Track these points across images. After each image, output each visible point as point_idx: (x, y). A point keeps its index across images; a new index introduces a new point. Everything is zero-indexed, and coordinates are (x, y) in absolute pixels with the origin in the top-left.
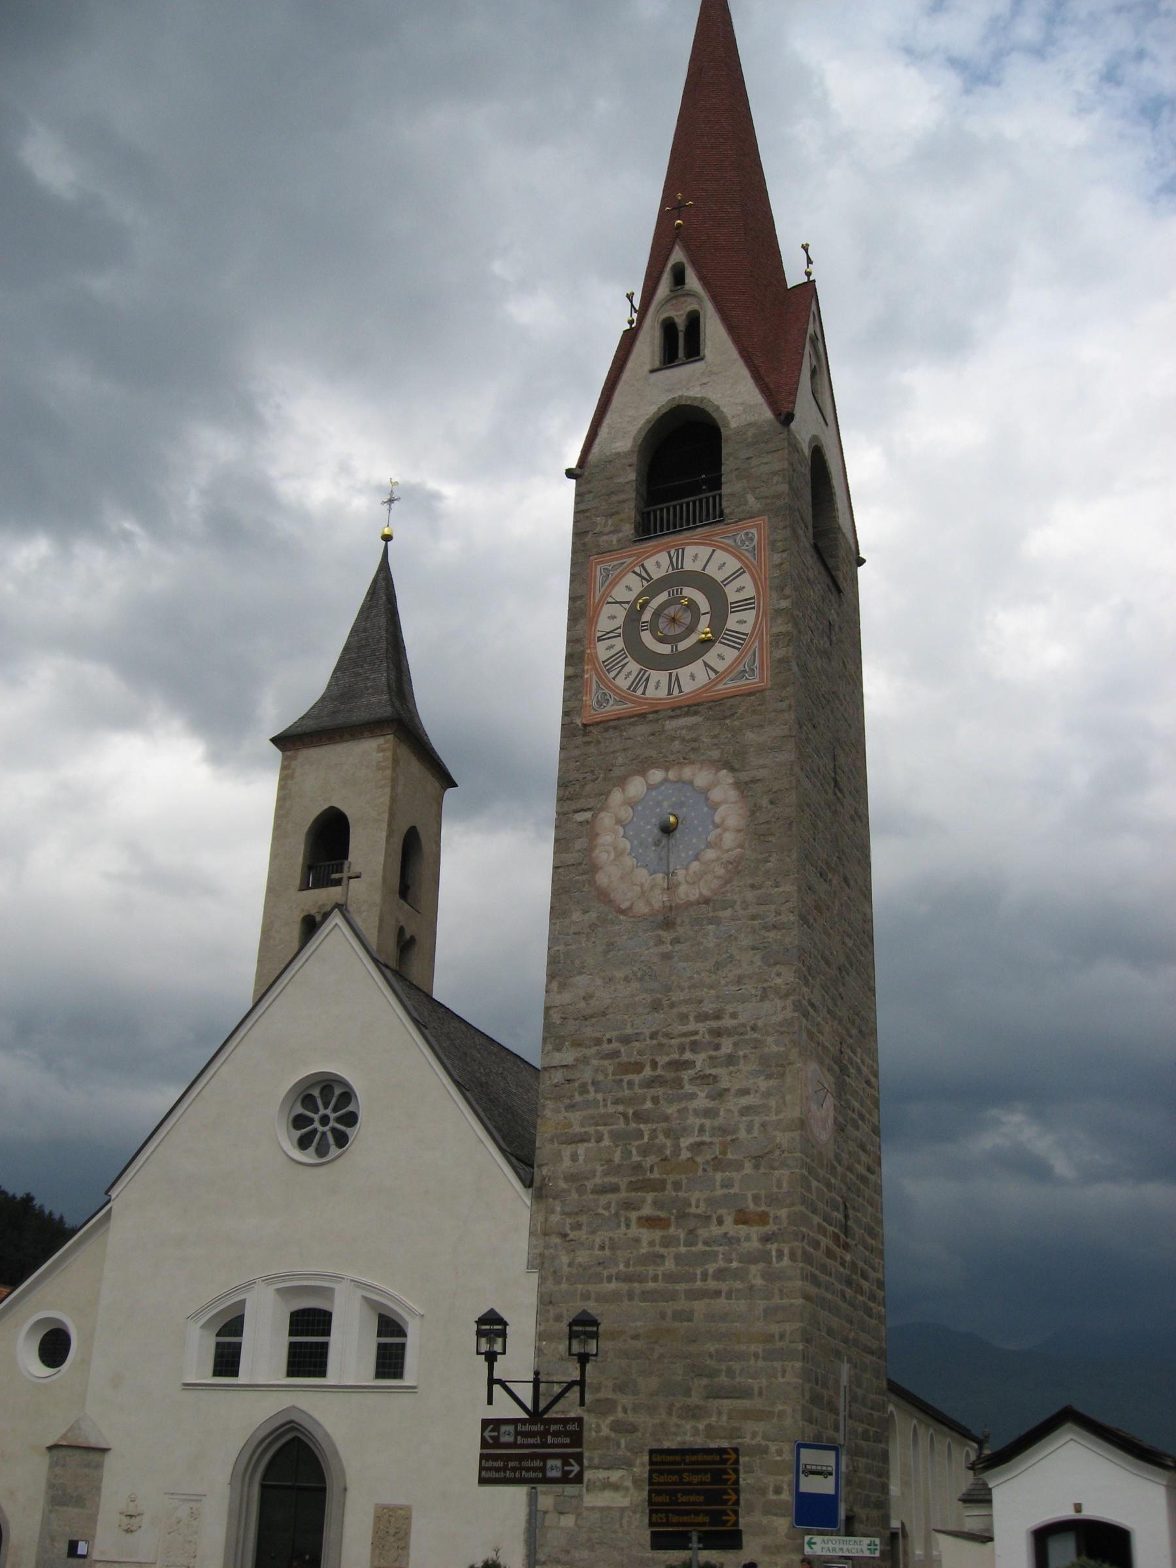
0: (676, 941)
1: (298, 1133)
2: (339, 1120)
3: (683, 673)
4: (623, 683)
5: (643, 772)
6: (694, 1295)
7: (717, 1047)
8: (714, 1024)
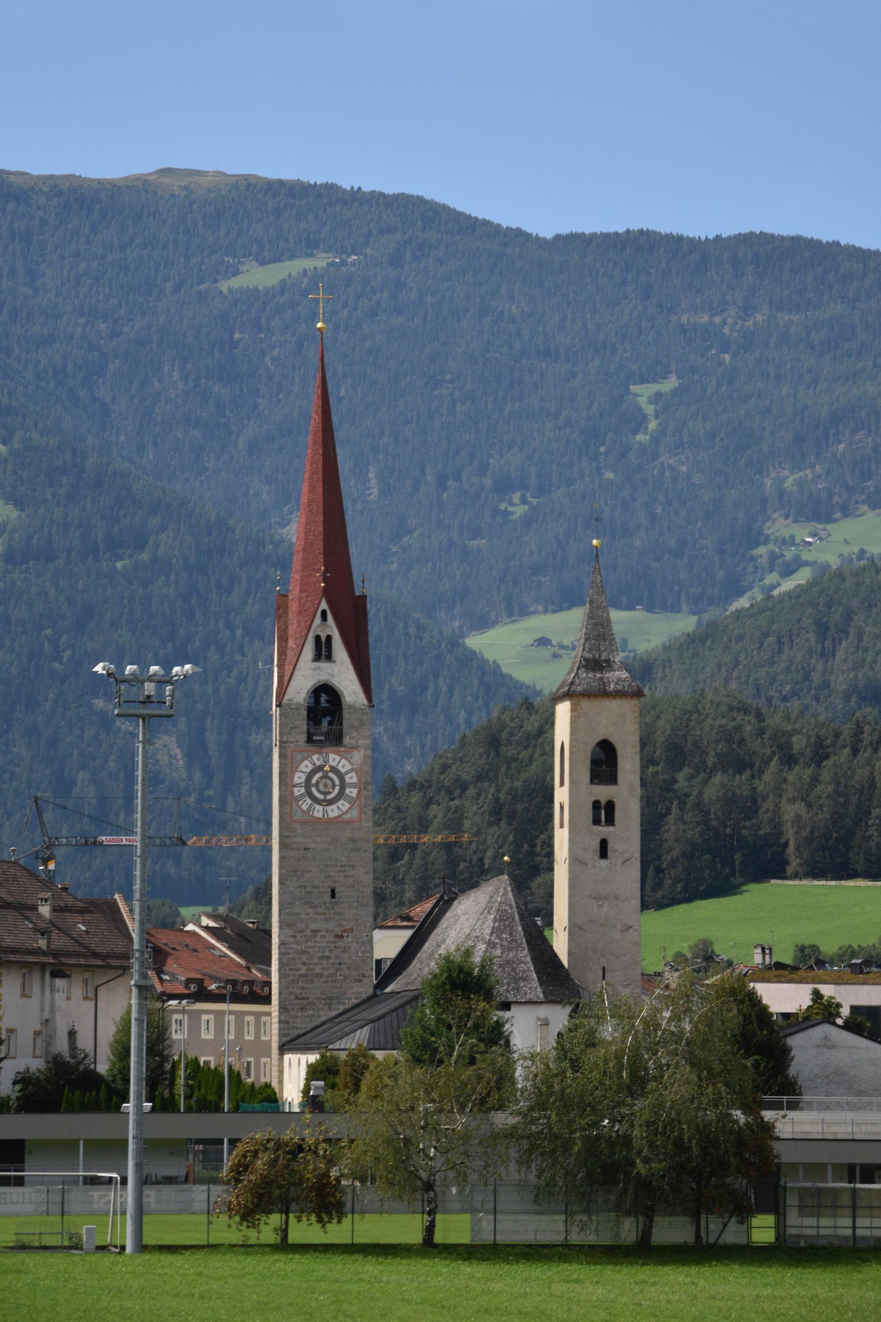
3: (329, 808)
4: (305, 807)
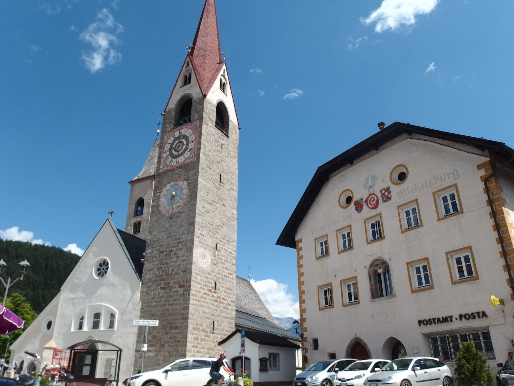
0: (173, 222)
1: (98, 272)
2: (100, 269)
3: (179, 159)
4: (168, 162)
5: (169, 183)
6: (169, 305)
7: (178, 246)
8: (178, 241)
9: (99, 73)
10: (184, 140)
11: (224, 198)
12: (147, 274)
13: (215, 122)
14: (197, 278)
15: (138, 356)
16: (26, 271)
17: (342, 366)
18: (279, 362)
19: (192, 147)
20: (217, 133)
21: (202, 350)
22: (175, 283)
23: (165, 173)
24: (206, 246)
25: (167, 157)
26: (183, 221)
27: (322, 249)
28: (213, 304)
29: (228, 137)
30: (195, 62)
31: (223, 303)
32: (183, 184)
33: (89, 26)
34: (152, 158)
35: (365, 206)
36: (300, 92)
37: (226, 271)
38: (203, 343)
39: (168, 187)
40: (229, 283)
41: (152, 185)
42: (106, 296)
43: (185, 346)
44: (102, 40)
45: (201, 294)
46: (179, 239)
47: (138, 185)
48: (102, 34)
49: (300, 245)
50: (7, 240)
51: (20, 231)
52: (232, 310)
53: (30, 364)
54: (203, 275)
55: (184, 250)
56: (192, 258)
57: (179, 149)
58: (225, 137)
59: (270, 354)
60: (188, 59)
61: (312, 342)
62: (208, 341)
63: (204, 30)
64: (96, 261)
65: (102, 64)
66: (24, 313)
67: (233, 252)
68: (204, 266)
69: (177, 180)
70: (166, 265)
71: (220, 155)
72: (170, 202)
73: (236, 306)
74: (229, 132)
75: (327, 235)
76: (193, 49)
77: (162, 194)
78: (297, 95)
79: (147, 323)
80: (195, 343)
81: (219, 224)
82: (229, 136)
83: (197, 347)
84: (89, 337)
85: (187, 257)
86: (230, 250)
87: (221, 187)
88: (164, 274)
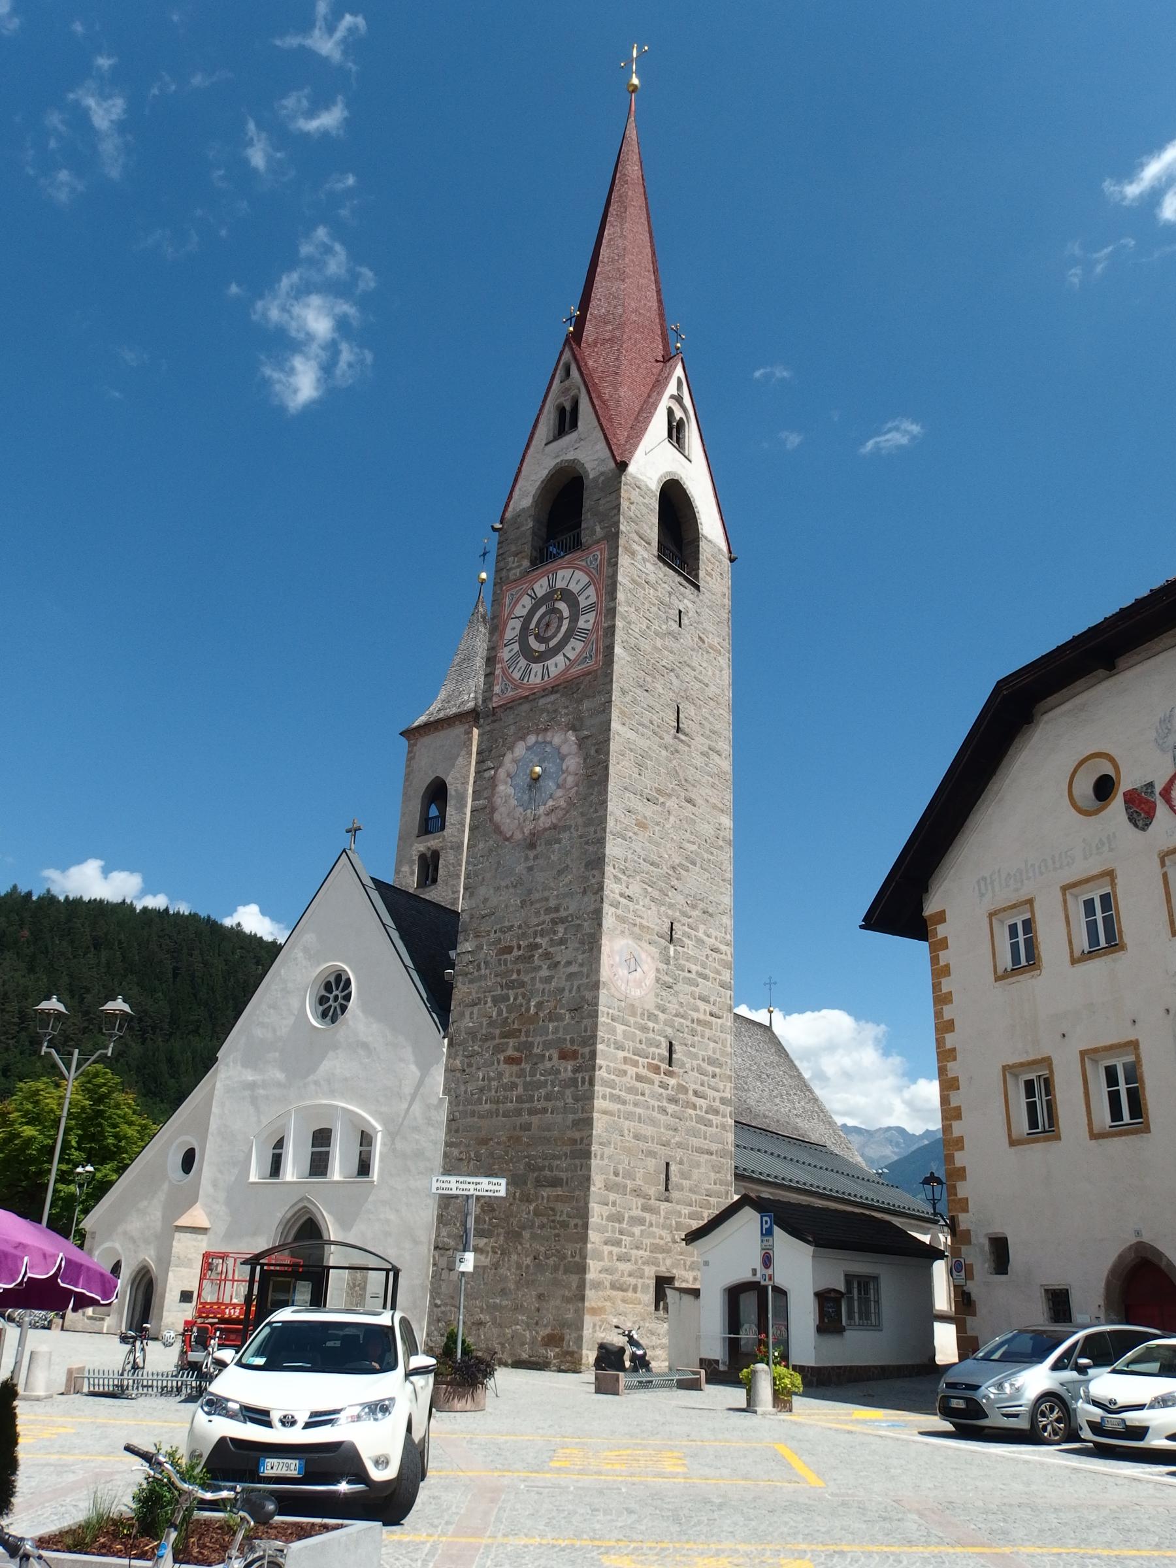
0: (536, 857)
1: (321, 1008)
3: (550, 663)
4: (516, 675)
5: (523, 738)
6: (532, 1112)
7: (555, 933)
8: (554, 915)
9: (311, 410)
10: (562, 606)
11: (690, 778)
12: (462, 1015)
13: (655, 544)
14: (613, 1031)
15: (443, 1262)
16: (120, 1029)
17: (1103, 1351)
18: (877, 1302)
19: (589, 626)
20: (664, 577)
21: (634, 1252)
22: (547, 1045)
23: (509, 707)
24: (638, 931)
25: (514, 660)
26: (567, 853)
27: (1015, 948)
28: (664, 1111)
29: (697, 587)
30: (590, 363)
31: (694, 1107)
32: (566, 741)
33: (279, 280)
34: (468, 659)
35: (1162, 810)
36: (915, 429)
37: (702, 1005)
38: (637, 1230)
39: (520, 749)
40: (712, 1045)
41: (471, 740)
42: (346, 1079)
43: (584, 1239)
44: (317, 321)
45: (629, 1080)
46: (557, 909)
47: (426, 740)
48: (315, 300)
49: (941, 930)
50: (67, 897)
51: (106, 871)
52: (724, 1127)
53: (138, 1273)
54: (632, 1020)
55: (572, 945)
56: (598, 971)
57: (550, 633)
58: (689, 591)
59: (849, 1279)
60: (567, 355)
61: (987, 1248)
62: (651, 1225)
63: (613, 261)
64: (315, 975)
65: (317, 389)
66: (119, 1120)
67: (723, 948)
68: (636, 993)
69: (546, 730)
70: (520, 991)
71: (675, 646)
72: (526, 797)
73: (737, 1113)
74: (702, 573)
75: (1030, 902)
76: (580, 323)
77: (502, 773)
78: (904, 441)
79: (472, 1187)
80: (612, 1228)
81: (677, 861)
82: (701, 584)
83: (618, 1243)
84: (301, 1200)
85: (581, 965)
86: (712, 941)
87: (681, 747)
88: (513, 1016)
